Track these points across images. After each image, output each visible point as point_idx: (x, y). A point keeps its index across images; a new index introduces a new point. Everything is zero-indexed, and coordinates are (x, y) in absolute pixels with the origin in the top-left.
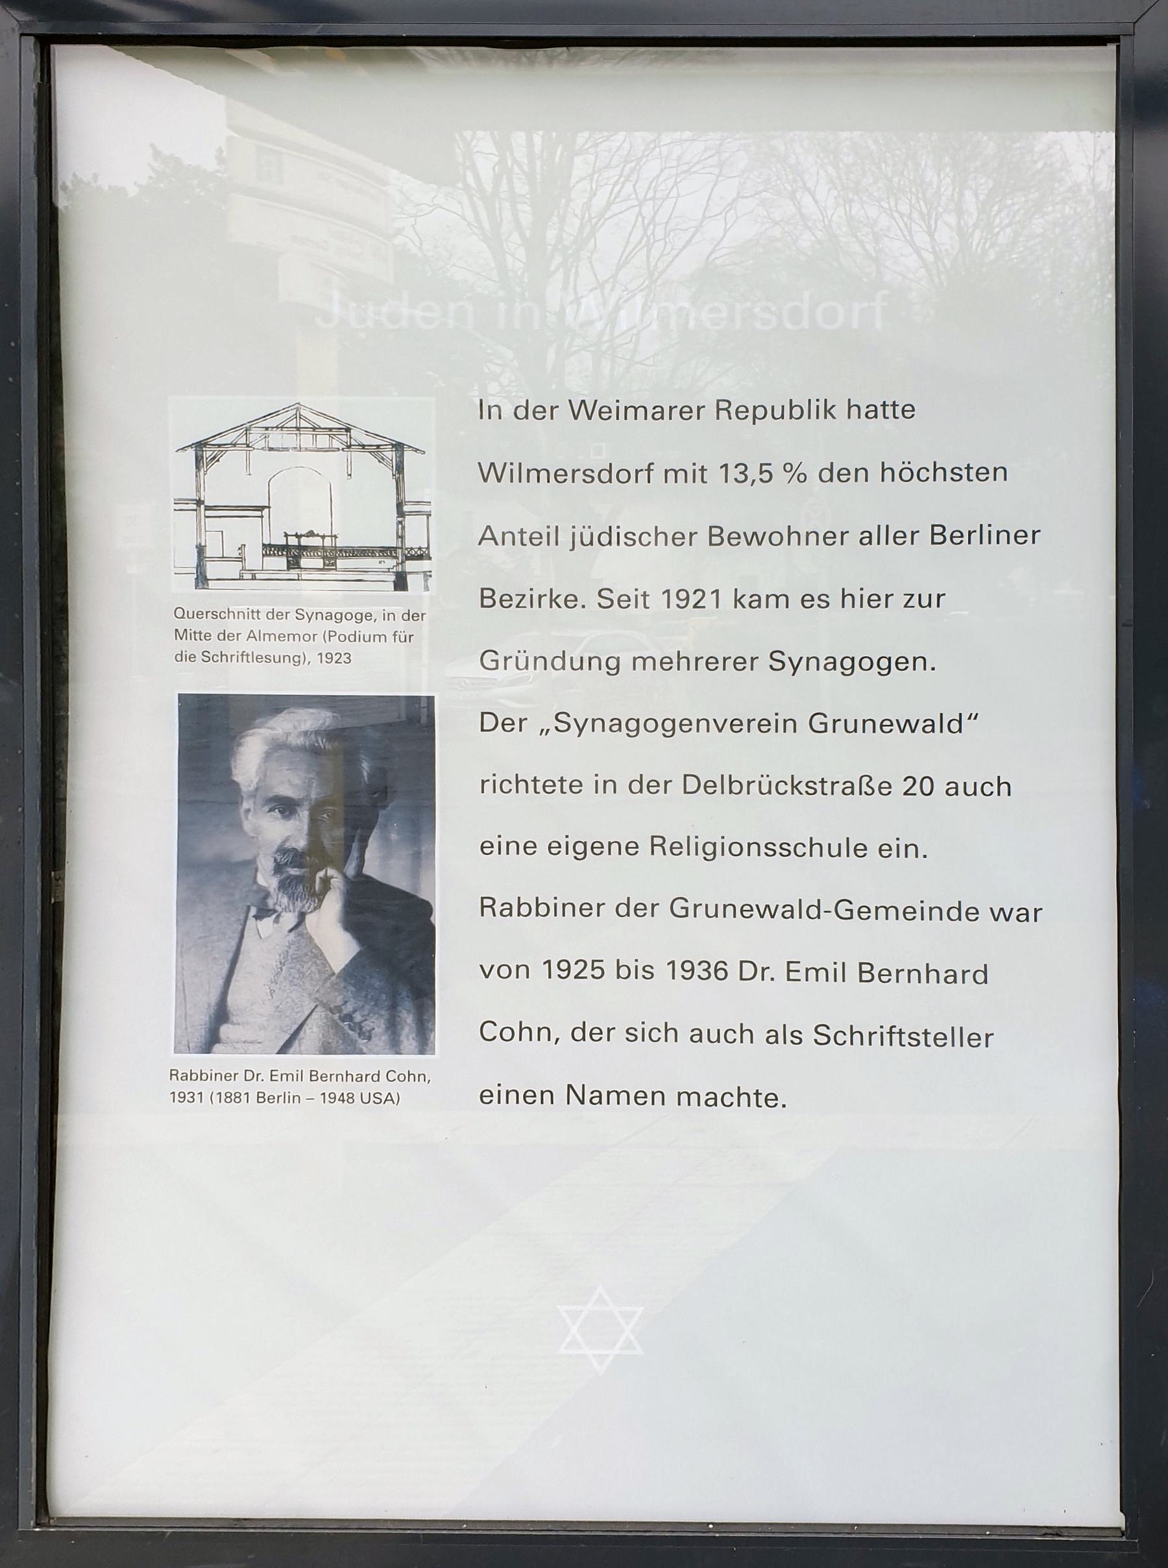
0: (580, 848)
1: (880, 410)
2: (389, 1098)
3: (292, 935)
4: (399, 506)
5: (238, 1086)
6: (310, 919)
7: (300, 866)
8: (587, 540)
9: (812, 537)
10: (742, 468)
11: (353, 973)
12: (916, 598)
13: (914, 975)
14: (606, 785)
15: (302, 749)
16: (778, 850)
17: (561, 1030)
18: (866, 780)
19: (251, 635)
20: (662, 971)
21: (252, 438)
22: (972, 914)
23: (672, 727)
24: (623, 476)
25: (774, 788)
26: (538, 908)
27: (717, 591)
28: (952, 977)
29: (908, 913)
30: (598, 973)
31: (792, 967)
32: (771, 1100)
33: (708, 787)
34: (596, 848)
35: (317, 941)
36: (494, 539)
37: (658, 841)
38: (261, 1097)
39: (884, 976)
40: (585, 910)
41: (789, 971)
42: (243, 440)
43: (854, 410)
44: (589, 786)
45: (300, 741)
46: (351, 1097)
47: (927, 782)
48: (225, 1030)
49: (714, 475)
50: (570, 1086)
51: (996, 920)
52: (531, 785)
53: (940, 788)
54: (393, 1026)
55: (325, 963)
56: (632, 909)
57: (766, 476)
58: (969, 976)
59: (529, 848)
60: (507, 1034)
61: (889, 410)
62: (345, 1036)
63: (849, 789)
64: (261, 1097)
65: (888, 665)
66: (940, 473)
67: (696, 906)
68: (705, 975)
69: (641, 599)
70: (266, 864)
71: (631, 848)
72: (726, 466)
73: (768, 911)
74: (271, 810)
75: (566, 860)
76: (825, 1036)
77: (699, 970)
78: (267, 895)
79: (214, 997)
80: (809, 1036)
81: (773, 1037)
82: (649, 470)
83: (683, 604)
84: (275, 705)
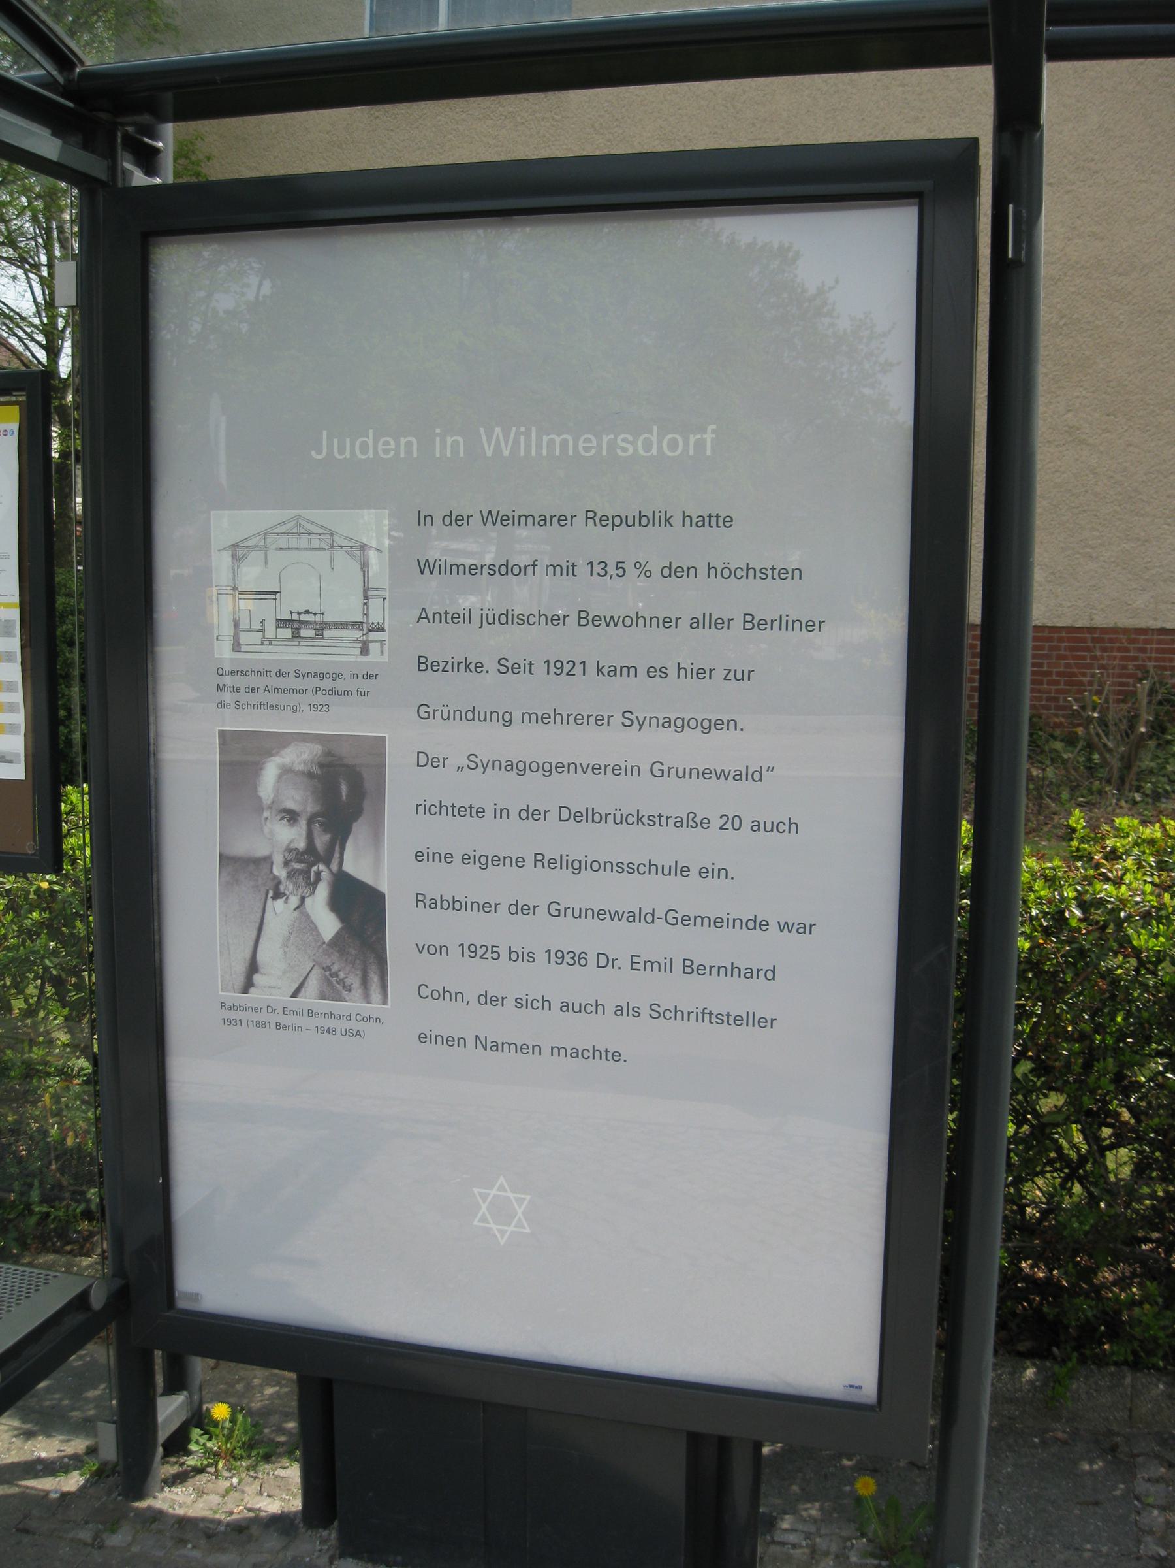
0: (483, 860)
1: (707, 520)
2: (358, 1034)
3: (296, 913)
4: (365, 591)
5: (262, 1016)
6: (308, 901)
7: (300, 862)
8: (491, 621)
9: (655, 621)
10: (603, 565)
11: (337, 942)
12: (732, 673)
13: (723, 970)
14: (502, 813)
15: (302, 773)
16: (626, 869)
17: (471, 996)
18: (691, 816)
19: (266, 690)
20: (542, 957)
21: (268, 541)
22: (763, 925)
23: (551, 769)
24: (516, 571)
25: (624, 820)
26: (454, 904)
27: (583, 662)
28: (750, 974)
29: (717, 922)
30: (495, 955)
31: (635, 959)
32: (616, 1056)
33: (576, 817)
34: (495, 860)
35: (313, 918)
36: (427, 618)
37: (539, 857)
38: (278, 1026)
39: (701, 970)
40: (486, 907)
41: (632, 962)
42: (262, 543)
43: (687, 520)
44: (489, 813)
45: (301, 767)
46: (334, 1030)
47: (737, 820)
48: (257, 978)
49: (582, 569)
50: (477, 1037)
51: (782, 931)
52: (450, 809)
53: (746, 825)
54: (365, 983)
55: (318, 934)
56: (519, 909)
57: (621, 572)
58: (762, 974)
59: (448, 858)
60: (435, 995)
61: (713, 520)
62: (332, 989)
63: (680, 823)
64: (278, 1026)
65: (708, 726)
66: (751, 572)
67: (566, 909)
68: (571, 962)
69: (528, 667)
70: (278, 859)
71: (519, 862)
72: (591, 563)
73: (616, 916)
74: (282, 819)
75: (474, 868)
76: (657, 1012)
77: (567, 958)
78: (279, 883)
79: (248, 954)
80: (645, 1011)
81: (619, 1011)
82: (534, 566)
83: (559, 671)
84: (282, 740)
